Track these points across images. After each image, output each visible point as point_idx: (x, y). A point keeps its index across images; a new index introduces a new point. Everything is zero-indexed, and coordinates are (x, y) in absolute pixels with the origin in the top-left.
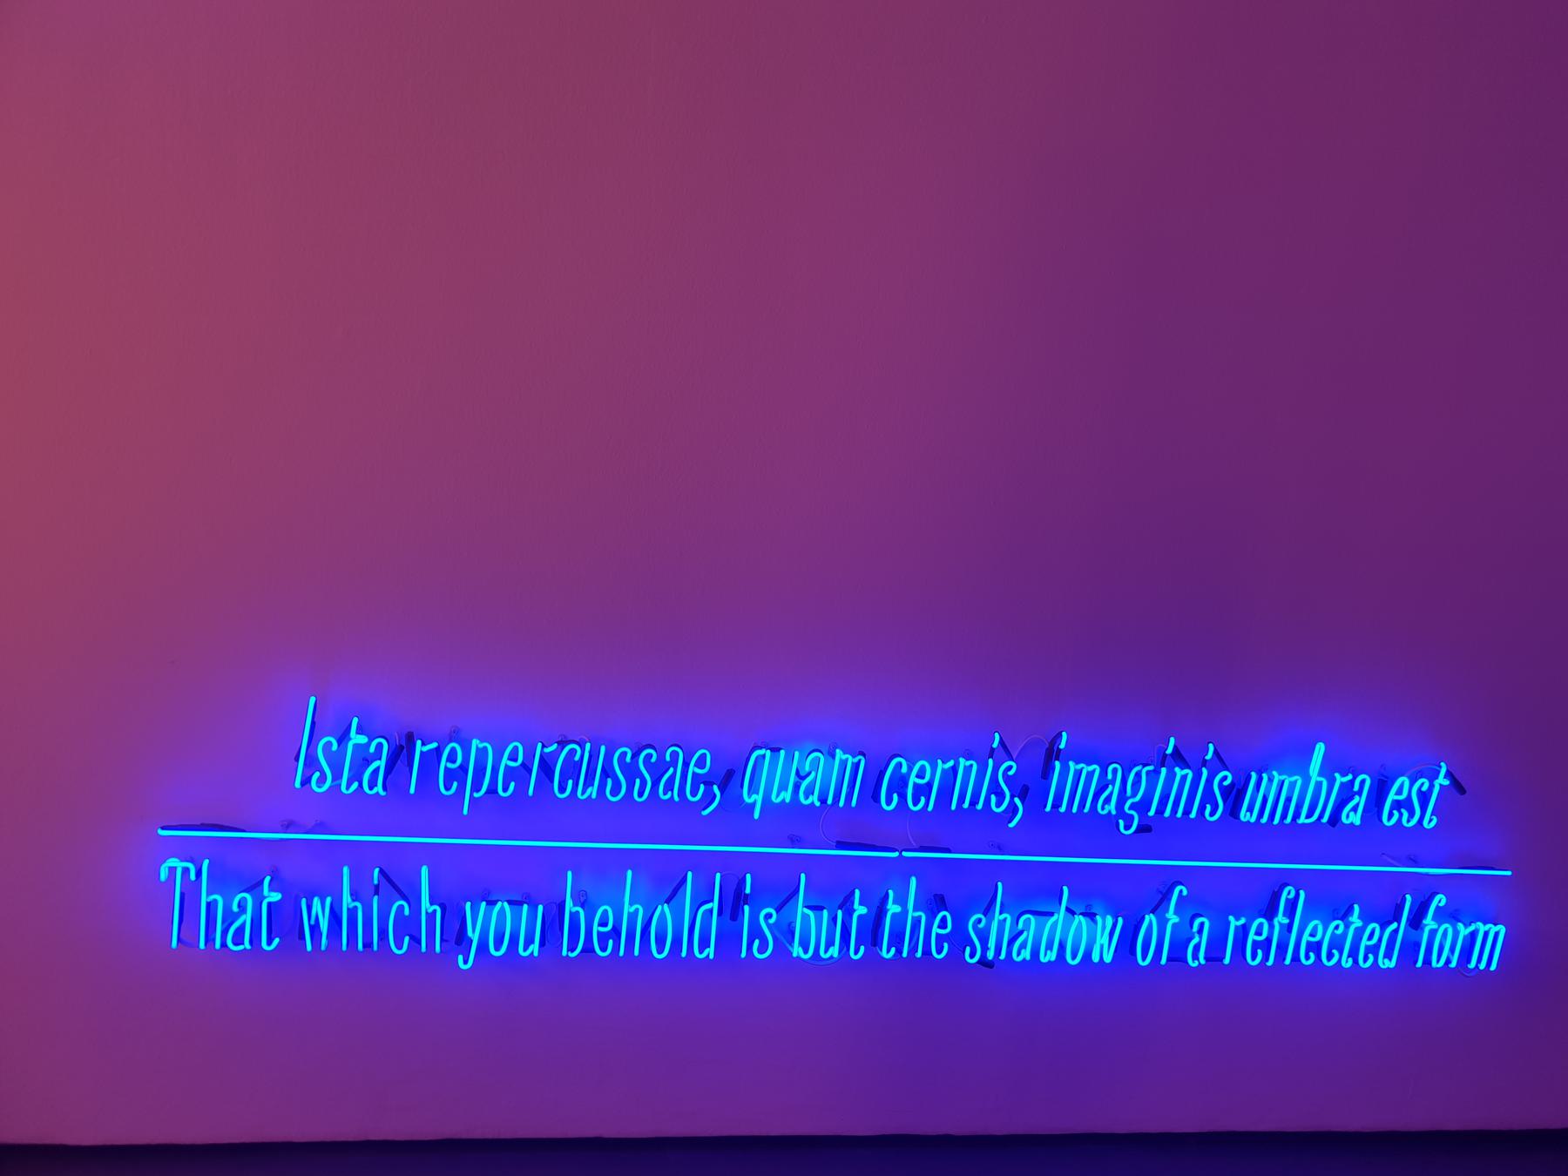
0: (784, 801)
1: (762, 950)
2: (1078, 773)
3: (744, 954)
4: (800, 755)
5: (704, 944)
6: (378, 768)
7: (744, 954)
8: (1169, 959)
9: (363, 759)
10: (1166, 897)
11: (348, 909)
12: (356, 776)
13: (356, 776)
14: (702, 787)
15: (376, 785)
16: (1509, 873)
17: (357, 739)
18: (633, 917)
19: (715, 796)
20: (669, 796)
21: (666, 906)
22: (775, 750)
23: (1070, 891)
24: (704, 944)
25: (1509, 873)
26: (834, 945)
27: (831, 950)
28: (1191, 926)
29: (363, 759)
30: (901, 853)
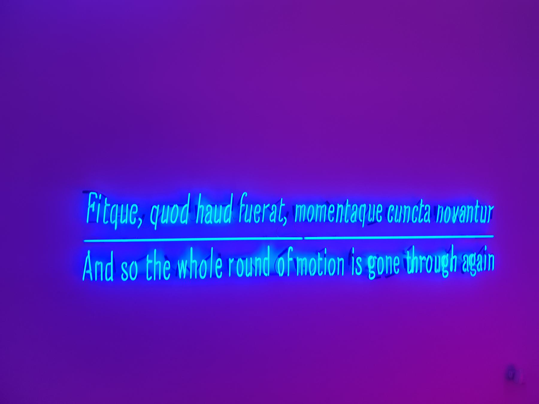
0: (165, 223)
1: (359, 271)
2: (319, 209)
3: (353, 274)
4: (253, 206)
5: (109, 276)
6: (209, 214)
7: (353, 274)
8: (212, 277)
9: (424, 212)
10: (286, 250)
11: (192, 264)
12: (422, 217)
13: (422, 217)
14: (135, 219)
15: (209, 219)
16: (492, 236)
17: (422, 206)
18: (194, 265)
19: (140, 222)
20: (427, 221)
21: (205, 261)
22: (120, 206)
23: (415, 247)
24: (109, 276)
25: (492, 236)
26: (250, 272)
27: (249, 273)
28: (463, 259)
29: (424, 212)
30: (303, 239)
